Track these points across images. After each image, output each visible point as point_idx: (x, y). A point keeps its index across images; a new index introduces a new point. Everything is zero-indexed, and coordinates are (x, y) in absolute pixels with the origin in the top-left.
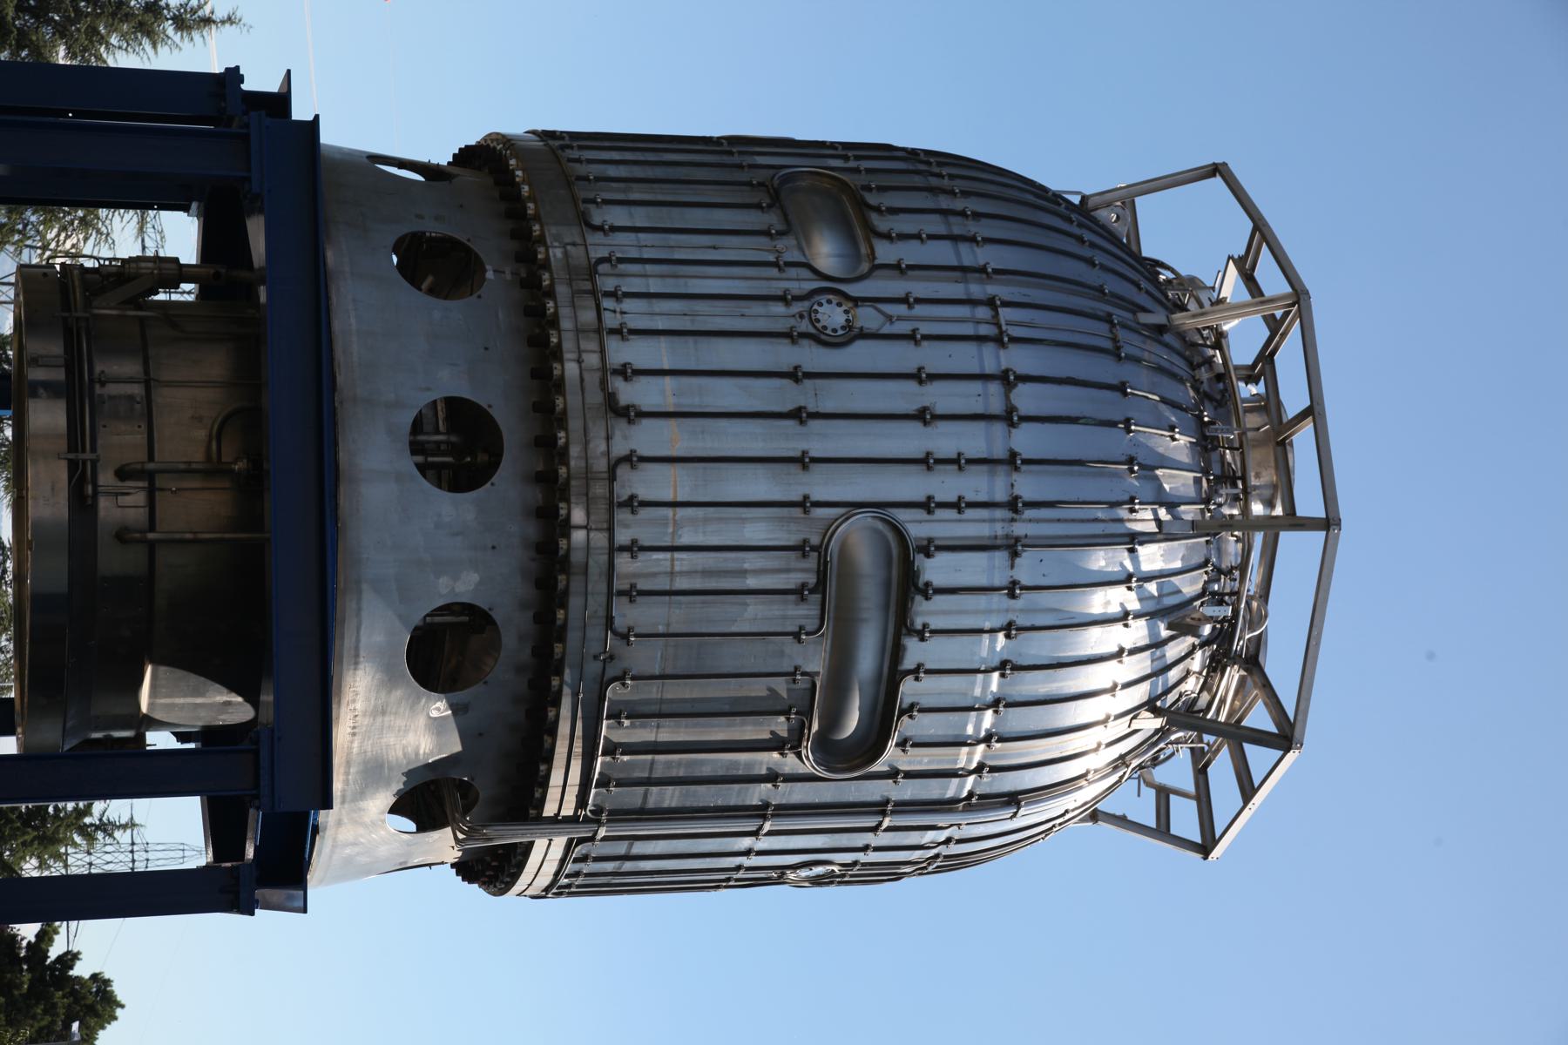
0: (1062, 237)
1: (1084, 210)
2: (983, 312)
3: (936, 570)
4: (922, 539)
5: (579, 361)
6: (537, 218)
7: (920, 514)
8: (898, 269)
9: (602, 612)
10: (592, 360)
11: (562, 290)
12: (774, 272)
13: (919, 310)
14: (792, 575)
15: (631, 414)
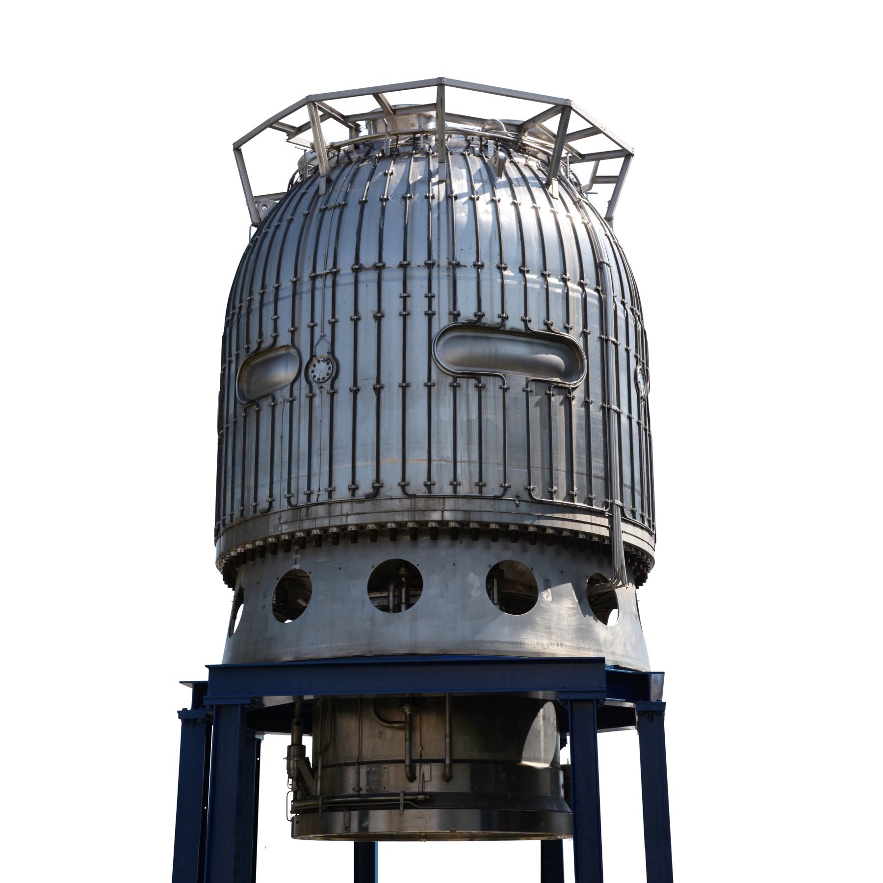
3: (467, 311)
5: (347, 515)
7: (435, 319)
9: (492, 502)
10: (346, 508)
11: (306, 525)
12: (296, 403)
13: (318, 320)
14: (470, 393)
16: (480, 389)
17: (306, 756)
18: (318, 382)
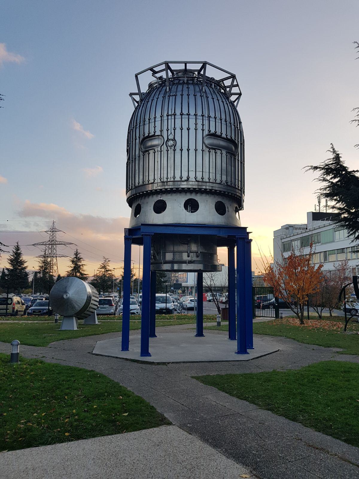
2: (170, 117)
3: (213, 131)
6: (139, 193)
7: (204, 131)
8: (161, 131)
9: (218, 185)
11: (166, 187)
12: (162, 152)
15: (188, 178)
16: (216, 153)
18: (170, 146)
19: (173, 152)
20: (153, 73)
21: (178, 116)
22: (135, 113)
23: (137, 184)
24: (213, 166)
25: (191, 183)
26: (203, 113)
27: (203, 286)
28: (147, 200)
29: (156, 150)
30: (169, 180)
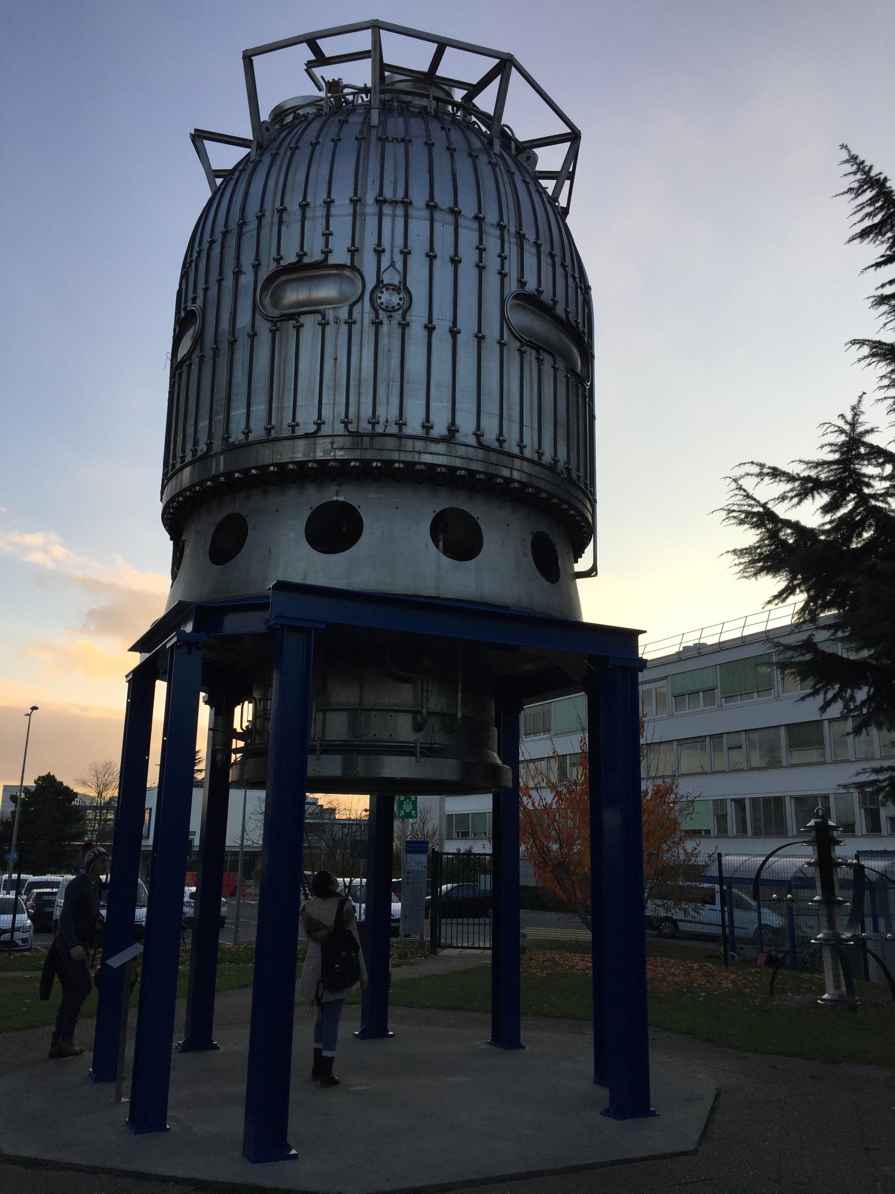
0: (232, 211)
1: (217, 192)
3: (531, 286)
4: (518, 285)
5: (420, 453)
8: (354, 251)
11: (369, 455)
12: (356, 328)
13: (386, 243)
14: (533, 363)
15: (453, 430)
17: (234, 727)
18: (386, 310)
19: (398, 331)
20: (313, 58)
21: (419, 213)
22: (220, 201)
23: (237, 436)
24: (531, 402)
25: (461, 451)
26: (501, 219)
27: (227, 849)
28: (292, 493)
29: (330, 315)
30: (380, 429)
